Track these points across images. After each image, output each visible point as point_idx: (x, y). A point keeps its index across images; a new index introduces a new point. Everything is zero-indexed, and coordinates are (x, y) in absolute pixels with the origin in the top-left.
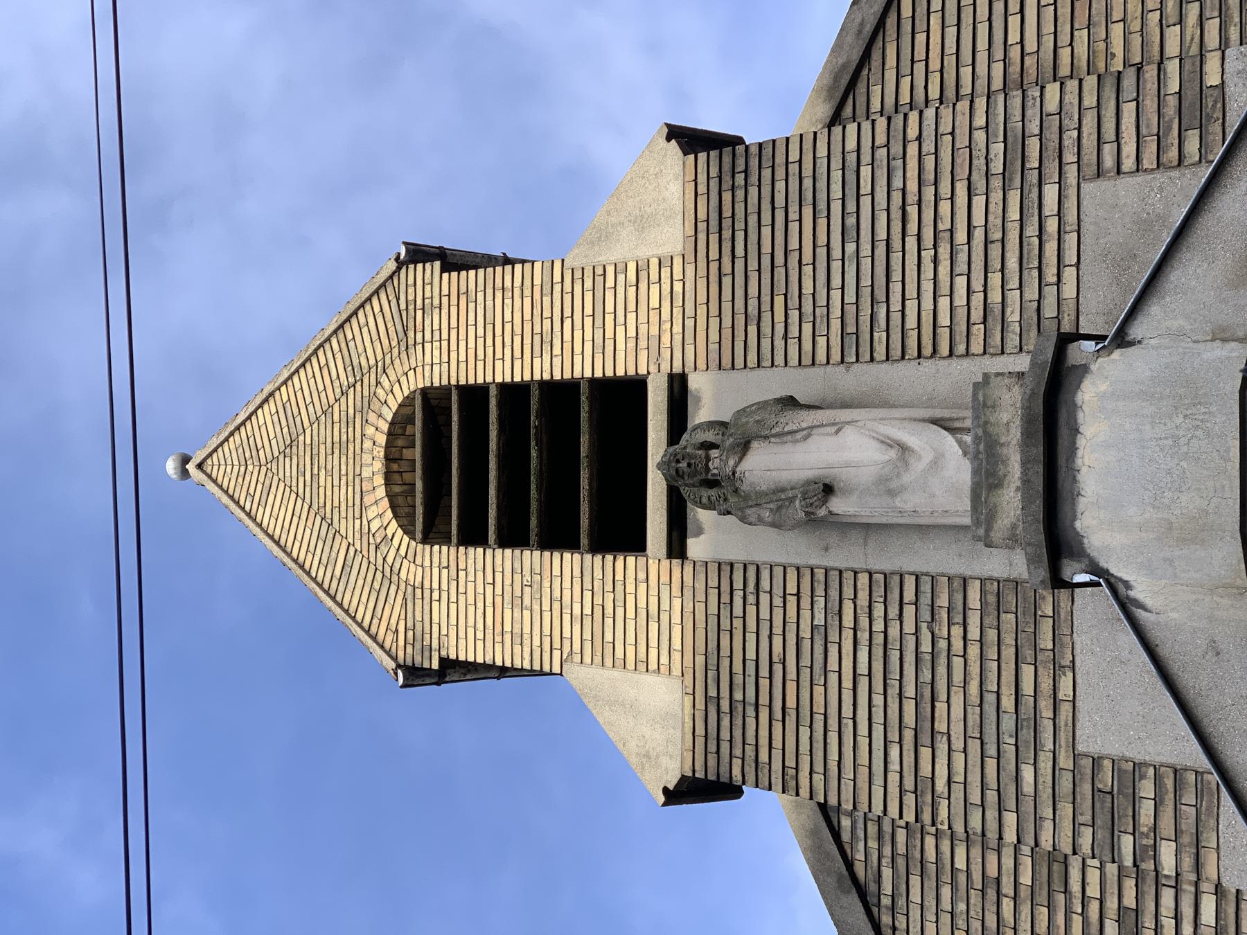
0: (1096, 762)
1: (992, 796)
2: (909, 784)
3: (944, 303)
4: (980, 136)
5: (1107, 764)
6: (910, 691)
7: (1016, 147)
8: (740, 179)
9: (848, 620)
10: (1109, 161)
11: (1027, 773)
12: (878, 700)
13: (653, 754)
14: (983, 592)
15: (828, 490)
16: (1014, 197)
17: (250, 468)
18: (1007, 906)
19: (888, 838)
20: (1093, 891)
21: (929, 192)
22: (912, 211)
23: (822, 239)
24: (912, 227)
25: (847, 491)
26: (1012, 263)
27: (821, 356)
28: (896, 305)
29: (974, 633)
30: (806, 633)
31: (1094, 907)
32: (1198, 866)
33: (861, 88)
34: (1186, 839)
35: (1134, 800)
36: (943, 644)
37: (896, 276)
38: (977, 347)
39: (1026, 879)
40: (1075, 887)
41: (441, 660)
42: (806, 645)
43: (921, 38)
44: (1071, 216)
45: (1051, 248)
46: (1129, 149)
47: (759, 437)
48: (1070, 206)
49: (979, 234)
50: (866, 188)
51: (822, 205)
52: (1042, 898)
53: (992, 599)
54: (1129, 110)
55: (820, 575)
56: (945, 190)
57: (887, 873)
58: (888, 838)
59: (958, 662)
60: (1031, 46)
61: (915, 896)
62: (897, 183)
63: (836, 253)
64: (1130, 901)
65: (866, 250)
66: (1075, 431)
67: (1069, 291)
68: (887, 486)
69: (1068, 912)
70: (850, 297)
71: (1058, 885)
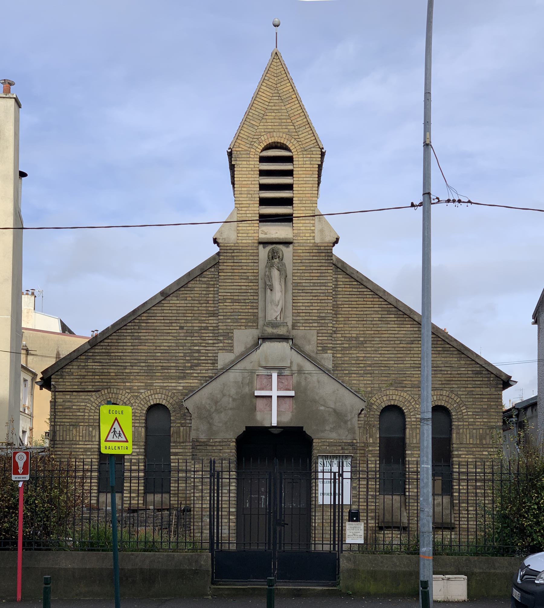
0: (232, 333)
1: (225, 314)
2: (225, 297)
3: (301, 304)
4: (326, 311)
5: (232, 335)
6: (240, 298)
7: (323, 318)
8: (327, 258)
9: (250, 284)
10: (319, 335)
11: (229, 321)
12: (237, 291)
13: (222, 235)
14: (256, 313)
15: (271, 290)
16: (316, 318)
17: (276, 79)
18: (205, 305)
19: (212, 280)
20: (210, 322)
21: (319, 301)
22: (316, 298)
23: (314, 278)
24: (314, 298)
25: (271, 294)
26: (306, 318)
27: (294, 278)
28: (302, 294)
29: (250, 311)
30: (247, 274)
31: (207, 322)
32: (220, 349)
33: (342, 273)
34: (224, 348)
35: (228, 339)
36: (247, 305)
37: (306, 295)
38: (294, 311)
39: (210, 309)
40: (210, 318)
41: (234, 165)
42: (245, 275)
43: (348, 286)
44: (312, 328)
45: (308, 325)
46: (321, 338)
47: (280, 273)
48: (314, 328)
49: (311, 311)
50: (322, 288)
51: (320, 278)
52: (208, 312)
53: (255, 314)
54: (326, 338)
55: (257, 278)
56: (319, 305)
57: (206, 279)
58: (212, 280)
59: (245, 307)
60: (343, 309)
61: (203, 286)
62: (321, 295)
63: (311, 281)
64: (210, 328)
65: (311, 288)
66: (279, 342)
67: (301, 328)
68: (272, 301)
69: (206, 317)
70: (304, 284)
71: (210, 315)
